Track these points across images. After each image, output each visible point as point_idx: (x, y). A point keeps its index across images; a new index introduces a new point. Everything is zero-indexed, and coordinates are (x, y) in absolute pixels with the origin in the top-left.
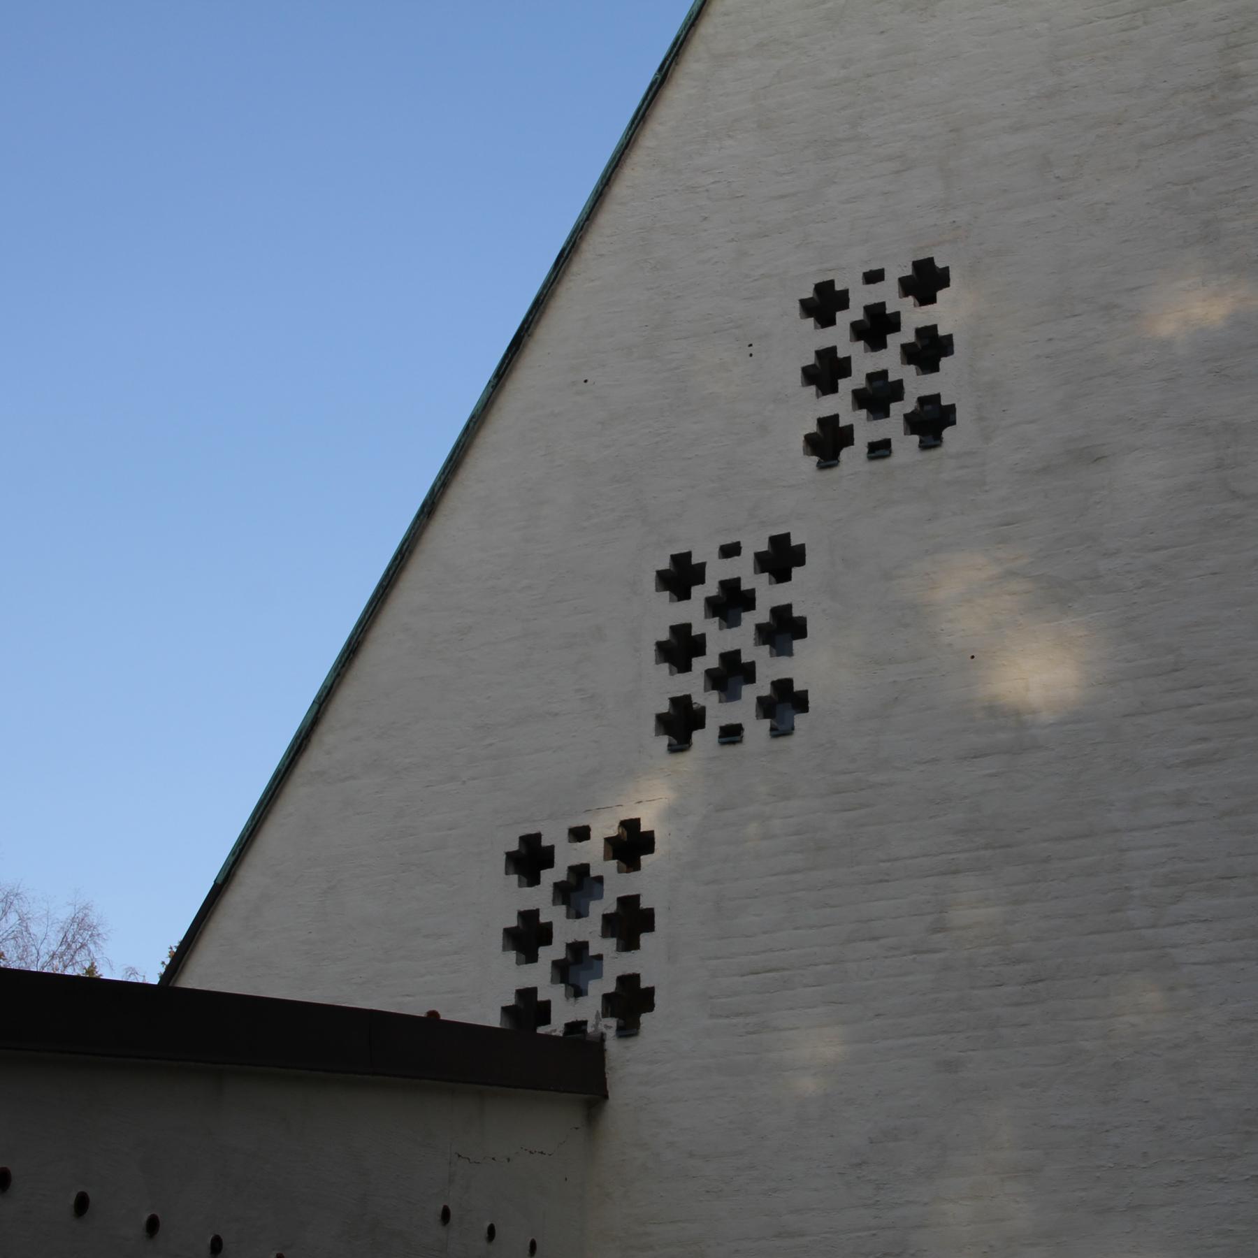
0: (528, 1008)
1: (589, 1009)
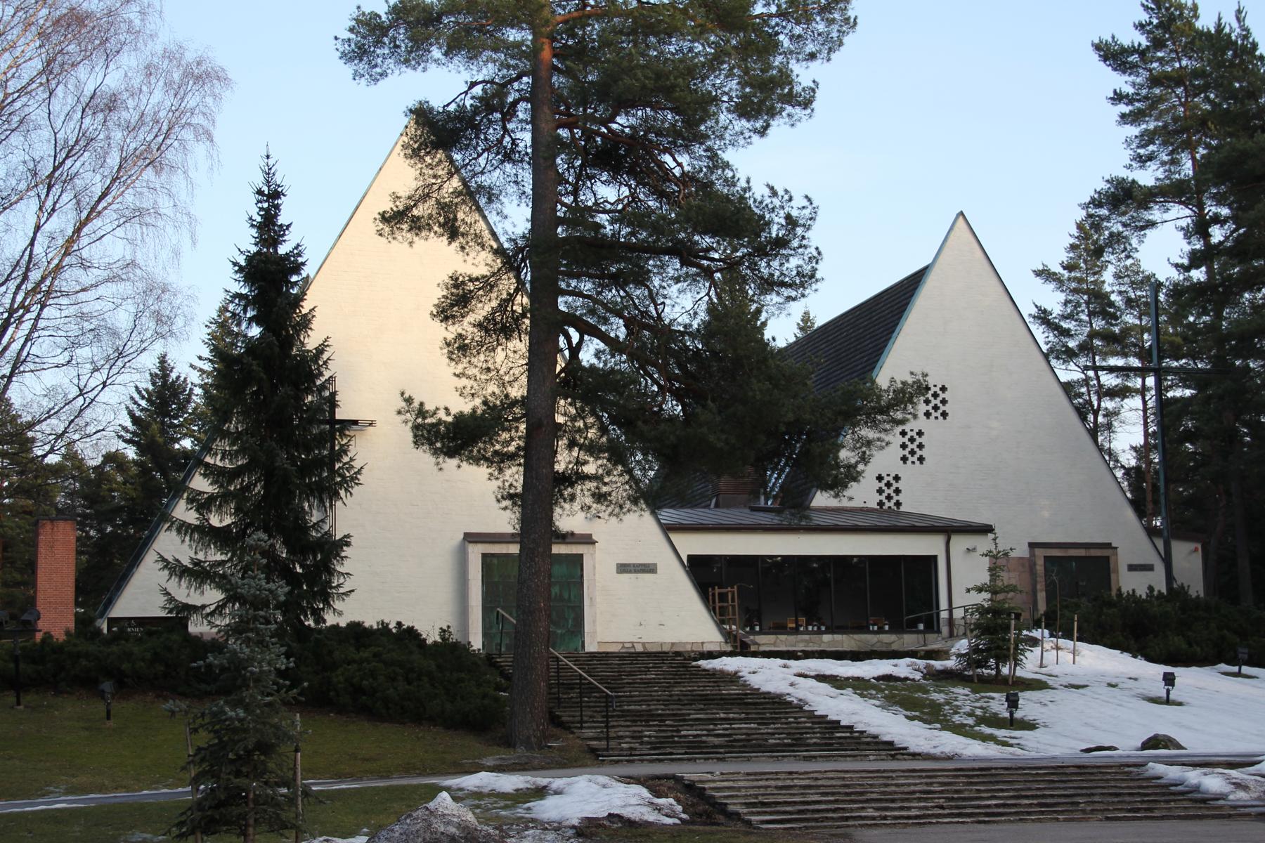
0: (881, 504)
1: (891, 504)
